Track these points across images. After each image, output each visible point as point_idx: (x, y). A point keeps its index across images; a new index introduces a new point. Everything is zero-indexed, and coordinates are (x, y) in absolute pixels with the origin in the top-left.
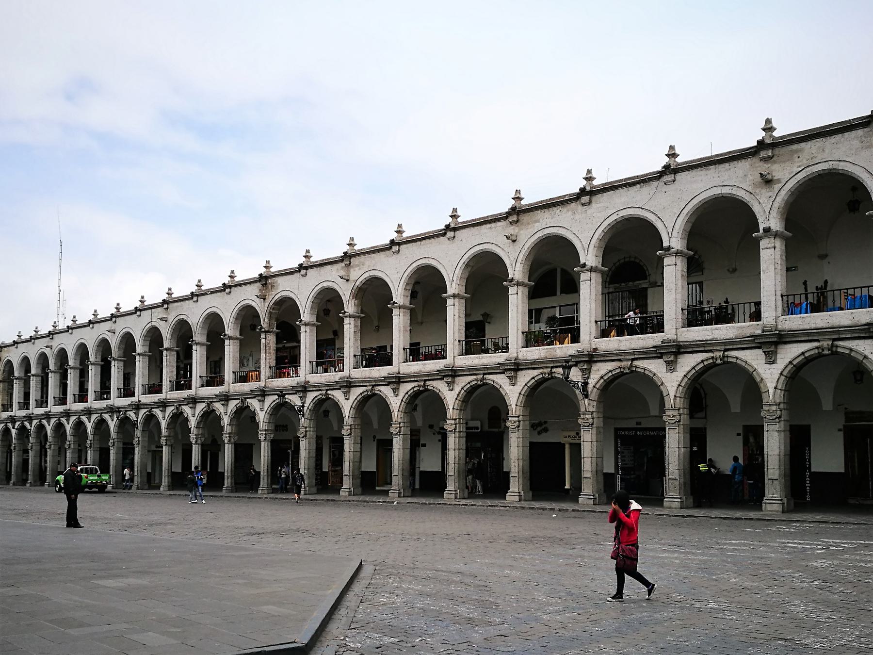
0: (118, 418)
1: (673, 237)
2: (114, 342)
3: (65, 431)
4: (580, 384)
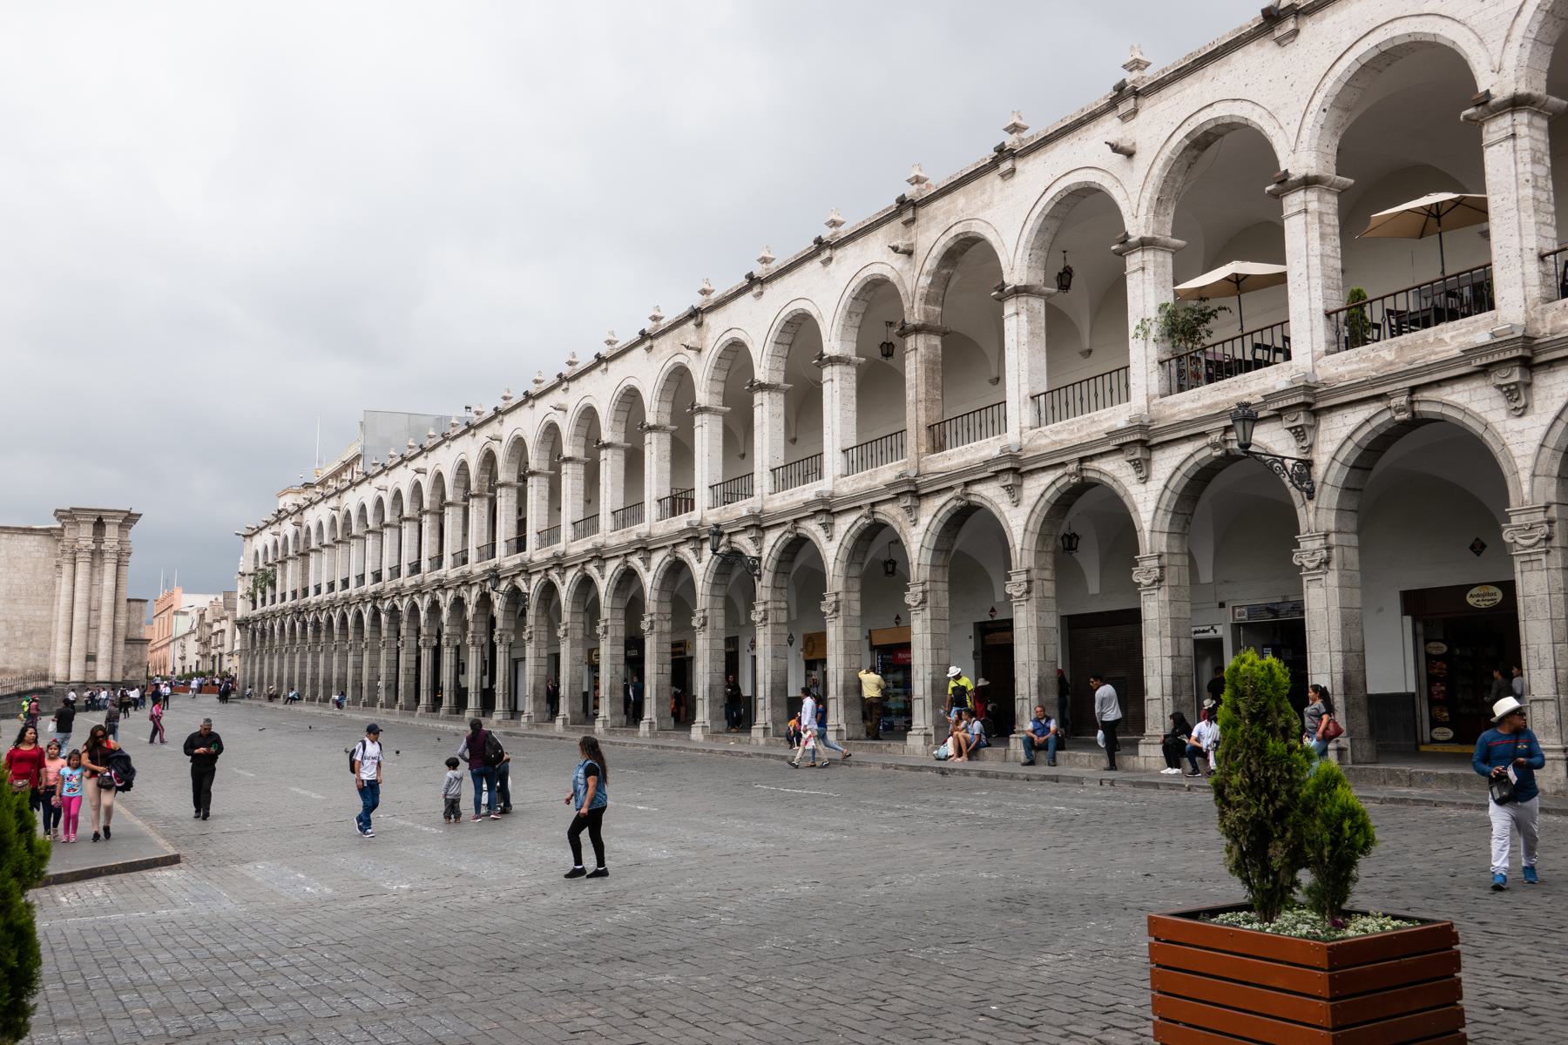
0: (714, 551)
1: (1301, 147)
2: (702, 372)
3: (641, 589)
4: (1289, 463)
